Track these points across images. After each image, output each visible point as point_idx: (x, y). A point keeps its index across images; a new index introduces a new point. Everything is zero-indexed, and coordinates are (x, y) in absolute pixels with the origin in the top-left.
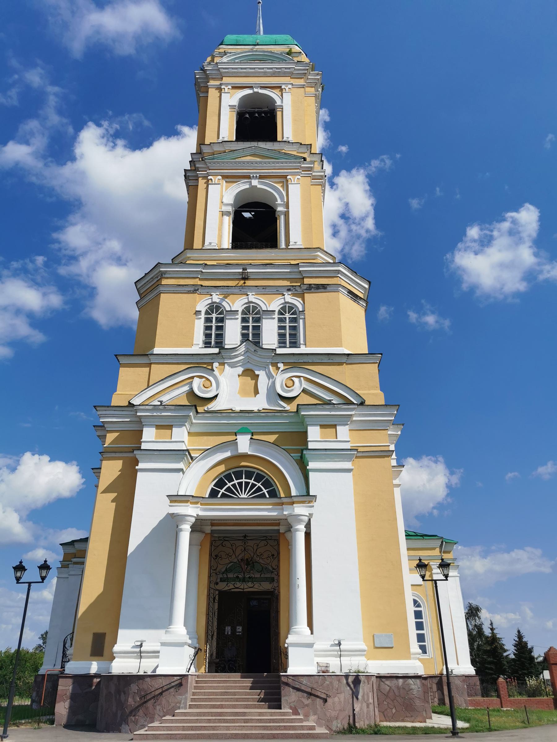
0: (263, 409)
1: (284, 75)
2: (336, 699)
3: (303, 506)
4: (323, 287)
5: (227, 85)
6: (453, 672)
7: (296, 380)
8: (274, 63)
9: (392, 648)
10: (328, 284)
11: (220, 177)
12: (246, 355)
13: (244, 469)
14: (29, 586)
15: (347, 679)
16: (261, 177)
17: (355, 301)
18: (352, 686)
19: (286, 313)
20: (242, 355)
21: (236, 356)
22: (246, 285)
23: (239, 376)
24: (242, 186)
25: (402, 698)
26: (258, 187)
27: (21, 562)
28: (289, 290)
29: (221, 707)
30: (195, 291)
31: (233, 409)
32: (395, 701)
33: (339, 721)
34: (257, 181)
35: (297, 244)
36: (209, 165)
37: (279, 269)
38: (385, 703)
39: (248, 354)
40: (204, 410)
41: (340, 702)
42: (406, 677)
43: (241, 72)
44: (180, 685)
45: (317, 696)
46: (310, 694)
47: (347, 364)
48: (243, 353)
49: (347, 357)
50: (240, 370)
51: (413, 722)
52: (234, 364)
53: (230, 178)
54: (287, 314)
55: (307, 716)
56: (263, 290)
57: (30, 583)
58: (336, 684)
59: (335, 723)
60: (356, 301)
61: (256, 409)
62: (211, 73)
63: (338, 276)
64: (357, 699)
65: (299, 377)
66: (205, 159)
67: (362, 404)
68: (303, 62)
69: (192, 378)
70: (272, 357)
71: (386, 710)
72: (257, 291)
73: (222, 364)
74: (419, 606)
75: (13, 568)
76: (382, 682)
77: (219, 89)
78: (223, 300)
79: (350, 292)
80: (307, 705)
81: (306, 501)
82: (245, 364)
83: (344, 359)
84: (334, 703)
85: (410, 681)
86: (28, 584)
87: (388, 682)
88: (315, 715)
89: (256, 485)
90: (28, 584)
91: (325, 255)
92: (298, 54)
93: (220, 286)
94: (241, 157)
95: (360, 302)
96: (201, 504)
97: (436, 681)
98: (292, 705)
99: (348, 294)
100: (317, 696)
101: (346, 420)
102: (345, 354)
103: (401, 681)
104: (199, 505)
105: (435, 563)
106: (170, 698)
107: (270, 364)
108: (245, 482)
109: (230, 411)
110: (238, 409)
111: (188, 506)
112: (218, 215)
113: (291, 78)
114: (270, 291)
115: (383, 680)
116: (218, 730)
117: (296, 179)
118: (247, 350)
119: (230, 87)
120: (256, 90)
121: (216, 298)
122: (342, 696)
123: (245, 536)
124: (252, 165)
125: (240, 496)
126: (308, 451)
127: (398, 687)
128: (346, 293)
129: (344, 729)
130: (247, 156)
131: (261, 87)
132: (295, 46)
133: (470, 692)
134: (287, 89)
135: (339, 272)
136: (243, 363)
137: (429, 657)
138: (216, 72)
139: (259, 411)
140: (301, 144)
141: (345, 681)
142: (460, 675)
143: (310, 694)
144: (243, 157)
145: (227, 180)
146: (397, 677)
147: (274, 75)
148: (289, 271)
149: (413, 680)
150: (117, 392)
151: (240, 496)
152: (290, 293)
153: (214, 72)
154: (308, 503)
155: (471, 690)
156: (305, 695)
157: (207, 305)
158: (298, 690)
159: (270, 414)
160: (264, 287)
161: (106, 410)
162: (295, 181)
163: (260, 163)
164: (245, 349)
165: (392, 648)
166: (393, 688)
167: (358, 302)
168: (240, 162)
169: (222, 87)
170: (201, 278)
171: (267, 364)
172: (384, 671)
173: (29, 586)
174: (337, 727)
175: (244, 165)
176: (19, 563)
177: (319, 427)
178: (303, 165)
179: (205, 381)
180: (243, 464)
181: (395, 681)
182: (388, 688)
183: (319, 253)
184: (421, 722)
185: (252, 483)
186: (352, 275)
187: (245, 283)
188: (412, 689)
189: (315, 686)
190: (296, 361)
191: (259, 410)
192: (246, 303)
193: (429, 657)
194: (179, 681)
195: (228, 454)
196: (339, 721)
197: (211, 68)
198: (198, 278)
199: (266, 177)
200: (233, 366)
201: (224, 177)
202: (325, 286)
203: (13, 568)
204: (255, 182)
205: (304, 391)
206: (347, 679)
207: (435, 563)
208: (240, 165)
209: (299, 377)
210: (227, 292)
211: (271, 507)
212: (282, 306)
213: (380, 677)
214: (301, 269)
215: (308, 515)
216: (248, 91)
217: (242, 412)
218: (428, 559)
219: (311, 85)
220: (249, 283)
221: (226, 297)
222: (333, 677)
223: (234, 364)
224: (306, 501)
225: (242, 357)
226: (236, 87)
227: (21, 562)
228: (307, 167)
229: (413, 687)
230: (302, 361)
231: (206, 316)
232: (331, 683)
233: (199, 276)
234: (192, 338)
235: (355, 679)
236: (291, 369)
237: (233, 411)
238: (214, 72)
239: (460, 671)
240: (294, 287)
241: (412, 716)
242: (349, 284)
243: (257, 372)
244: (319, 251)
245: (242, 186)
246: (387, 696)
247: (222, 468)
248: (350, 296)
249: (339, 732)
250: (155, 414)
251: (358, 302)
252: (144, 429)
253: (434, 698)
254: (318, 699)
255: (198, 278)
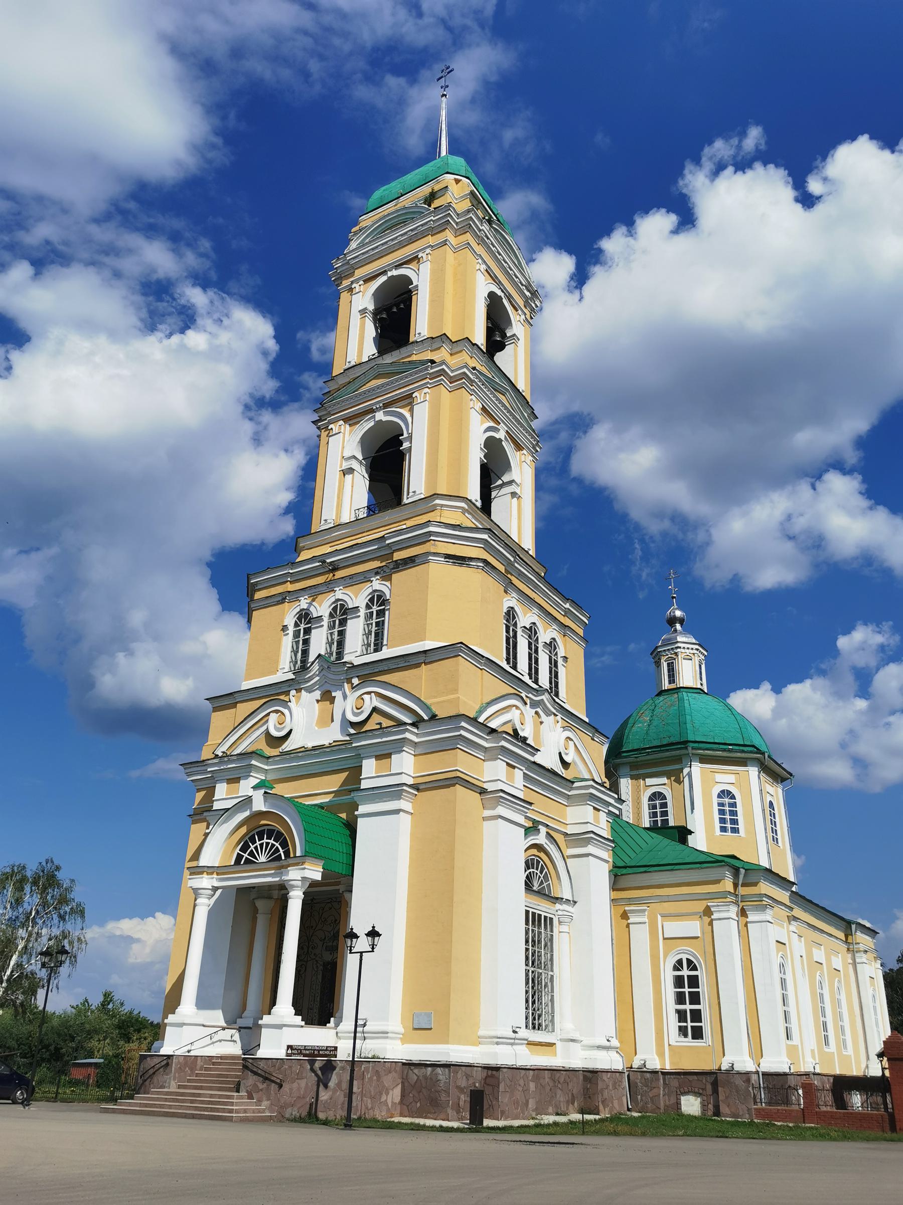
0: (334, 741)
1: (412, 240)
2: (295, 1085)
3: (297, 869)
4: (410, 562)
5: (357, 281)
6: (734, 1066)
7: (366, 697)
8: (408, 224)
9: (431, 1029)
10: (415, 556)
11: (341, 422)
12: (322, 674)
13: (266, 828)
14: (361, 957)
15: (312, 1063)
16: (386, 406)
17: (461, 565)
18: (319, 1073)
19: (373, 606)
20: (317, 675)
21: (311, 678)
22: (336, 577)
23: (318, 701)
24: (367, 425)
25: (429, 1090)
26: (384, 420)
27: (373, 927)
28: (377, 573)
29: (201, 1088)
30: (282, 601)
31: (306, 747)
32: (421, 1093)
33: (296, 1109)
34: (382, 412)
35: (417, 493)
36: (330, 409)
37: (366, 547)
38: (411, 1095)
39: (324, 672)
40: (280, 752)
41: (299, 1089)
42: (434, 1065)
43: (373, 254)
44: (167, 1064)
45: (273, 1081)
46: (266, 1079)
47: (426, 664)
48: (317, 673)
49: (424, 655)
50: (317, 694)
51: (435, 1119)
52: (310, 687)
53: (352, 420)
54: (375, 607)
55: (259, 1101)
56: (351, 581)
57: (361, 953)
58: (297, 1068)
59: (289, 1110)
60: (464, 564)
61: (326, 743)
62: (343, 270)
63: (431, 540)
64: (326, 1086)
65: (369, 693)
66: (325, 403)
67: (433, 717)
68: (442, 206)
69: (268, 714)
70: (345, 672)
71: (411, 1103)
72: (344, 583)
73: (299, 690)
74: (695, 968)
75: (366, 934)
76: (411, 1070)
77: (350, 290)
78: (310, 604)
79: (448, 556)
80: (261, 1090)
81: (299, 863)
82: (323, 685)
83: (421, 659)
84: (291, 1089)
85: (439, 1070)
86: (359, 954)
87: (416, 1071)
88: (268, 1100)
89: (252, 850)
90: (359, 954)
91: (450, 500)
92: (444, 190)
93: (307, 588)
94: (364, 385)
95: (471, 563)
96: (218, 874)
97: (711, 1079)
98: (248, 1088)
99: (448, 560)
100: (273, 1081)
101: (399, 746)
102: (420, 652)
103: (429, 1069)
104: (215, 876)
105: (716, 904)
106: (159, 1078)
107: (346, 680)
108: (266, 843)
109: (303, 749)
110: (310, 745)
111: (202, 878)
112: (338, 475)
113: (432, 236)
114: (358, 579)
115: (412, 1068)
116: (163, 1108)
117: (423, 394)
118: (321, 668)
119: (362, 282)
120: (390, 274)
121: (304, 603)
122: (303, 1083)
123: (312, 900)
124: (374, 392)
125: (258, 860)
126: (359, 792)
127: (425, 1077)
128: (443, 559)
129: (300, 1117)
130: (371, 380)
131: (396, 266)
132: (445, 175)
133: (774, 1098)
134: (424, 255)
135: (430, 533)
136: (320, 685)
137: (705, 1045)
138: (347, 267)
139: (330, 746)
140: (432, 338)
141: (309, 1067)
142: (743, 1072)
143: (266, 1079)
144: (367, 383)
145: (351, 422)
146: (426, 1065)
147: (402, 245)
148: (376, 547)
149: (442, 1069)
150: (209, 743)
151: (258, 860)
152: (378, 577)
153: (344, 268)
154: (302, 865)
155: (776, 1096)
156: (262, 1079)
157: (296, 614)
158: (255, 1073)
159: (343, 747)
160: (351, 577)
161: (190, 768)
162: (422, 398)
163: (387, 384)
164: (318, 667)
165: (431, 1029)
166: (421, 1078)
167: (467, 564)
168: (360, 394)
169: (353, 287)
170: (292, 580)
171: (343, 681)
172: (415, 1058)
173: (361, 957)
174: (292, 1115)
175: (365, 395)
176: (372, 929)
177: (374, 759)
178: (432, 371)
179: (280, 715)
180: (263, 822)
181: (423, 1070)
182: (415, 1078)
183: (438, 502)
184: (443, 1120)
185: (260, 845)
186: (454, 530)
187: (334, 575)
188: (439, 1080)
189: (272, 1070)
190: (371, 672)
191: (330, 744)
192: (334, 603)
193: (705, 1045)
194: (165, 1062)
195: (247, 813)
196: (296, 1109)
197: (340, 264)
198: (287, 581)
199: (390, 403)
200: (310, 690)
201: (346, 420)
202: (413, 558)
203: (366, 934)
204: (380, 416)
205: (375, 710)
206: (312, 1063)
207: (716, 904)
208: (361, 397)
209: (369, 693)
210: (315, 592)
211: (273, 872)
212: (370, 596)
213: (409, 1065)
214: (388, 542)
215: (300, 879)
216: (383, 279)
217: (314, 748)
218: (697, 898)
219: (464, 230)
220: (339, 574)
221: (313, 600)
222: (293, 1061)
223: (310, 687)
224: (299, 863)
225: (318, 678)
226: (368, 280)
227: (373, 927)
228: (437, 371)
229: (441, 1077)
230: (377, 670)
231: (295, 629)
232: (290, 1067)
233: (289, 579)
234: (277, 662)
235: (325, 1065)
236: (363, 684)
237: (322, 747)
238: (344, 268)
239: (745, 1066)
240: (382, 569)
241: (435, 1113)
242: (454, 543)
243: (334, 694)
244: (437, 498)
245: (367, 425)
246: (413, 1086)
247: (244, 830)
248: (451, 561)
249: (288, 1120)
250: (222, 768)
251: (467, 564)
252: (217, 785)
253: (708, 1104)
254: (273, 1084)
255: (287, 581)
